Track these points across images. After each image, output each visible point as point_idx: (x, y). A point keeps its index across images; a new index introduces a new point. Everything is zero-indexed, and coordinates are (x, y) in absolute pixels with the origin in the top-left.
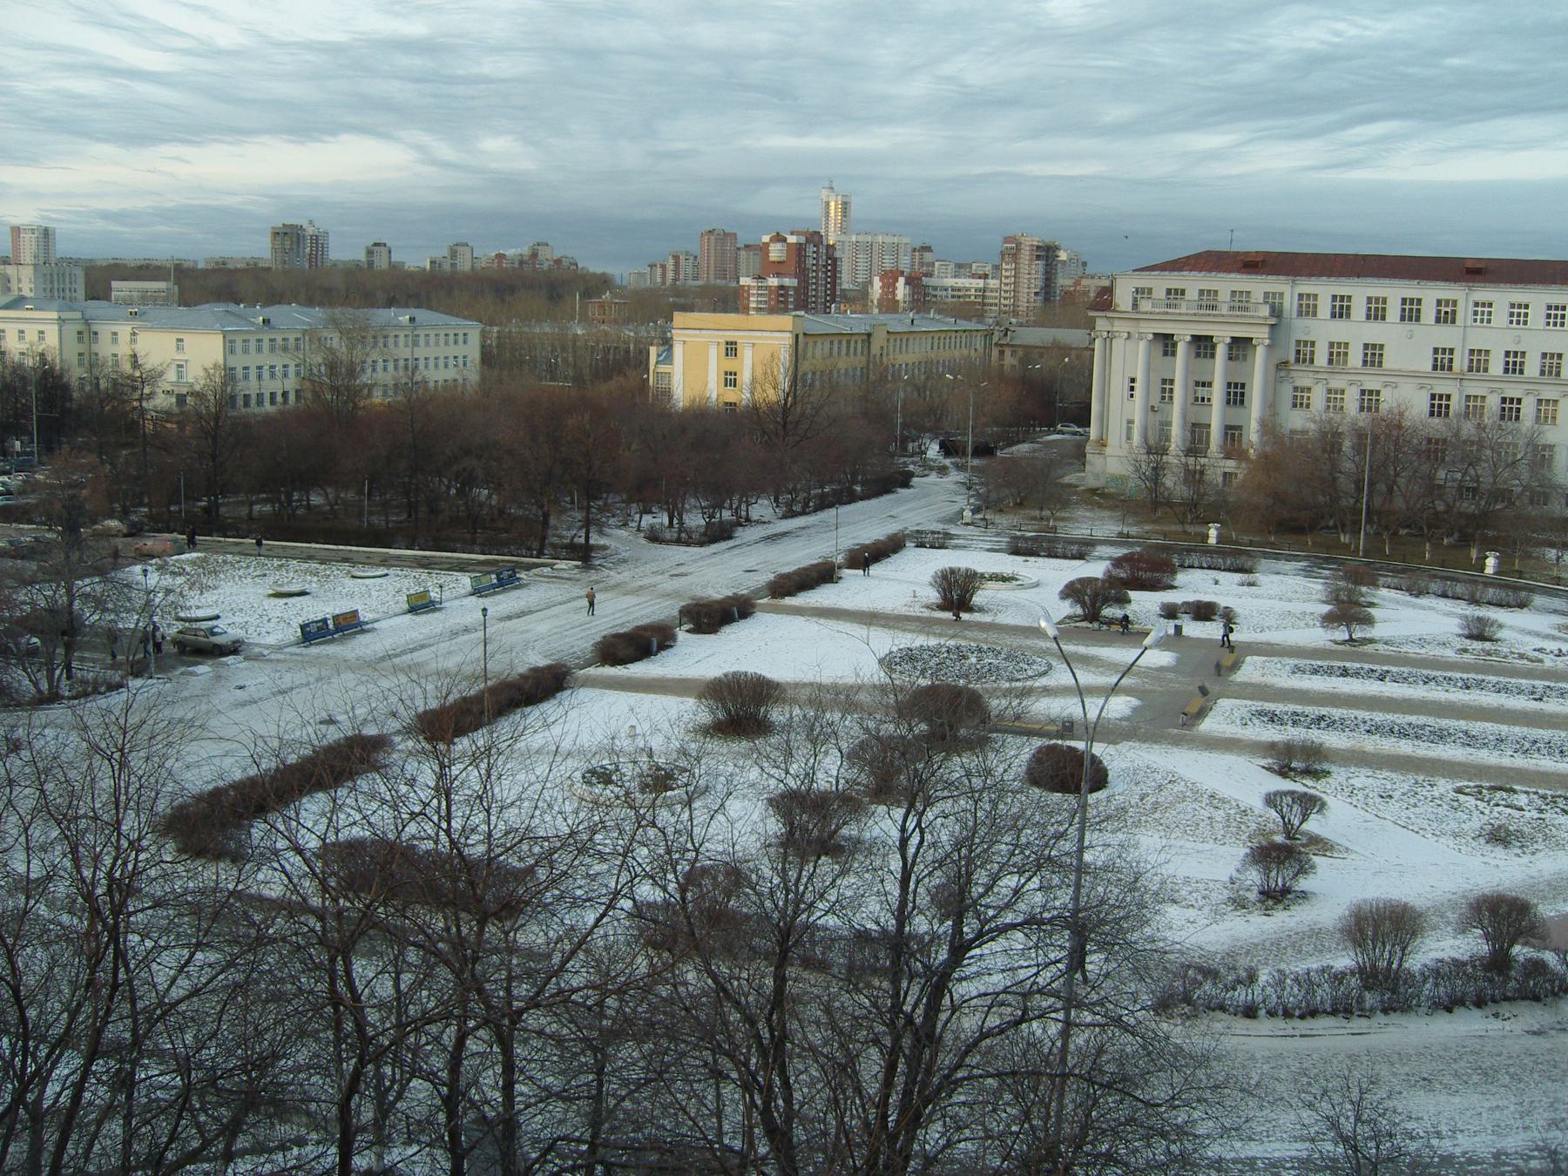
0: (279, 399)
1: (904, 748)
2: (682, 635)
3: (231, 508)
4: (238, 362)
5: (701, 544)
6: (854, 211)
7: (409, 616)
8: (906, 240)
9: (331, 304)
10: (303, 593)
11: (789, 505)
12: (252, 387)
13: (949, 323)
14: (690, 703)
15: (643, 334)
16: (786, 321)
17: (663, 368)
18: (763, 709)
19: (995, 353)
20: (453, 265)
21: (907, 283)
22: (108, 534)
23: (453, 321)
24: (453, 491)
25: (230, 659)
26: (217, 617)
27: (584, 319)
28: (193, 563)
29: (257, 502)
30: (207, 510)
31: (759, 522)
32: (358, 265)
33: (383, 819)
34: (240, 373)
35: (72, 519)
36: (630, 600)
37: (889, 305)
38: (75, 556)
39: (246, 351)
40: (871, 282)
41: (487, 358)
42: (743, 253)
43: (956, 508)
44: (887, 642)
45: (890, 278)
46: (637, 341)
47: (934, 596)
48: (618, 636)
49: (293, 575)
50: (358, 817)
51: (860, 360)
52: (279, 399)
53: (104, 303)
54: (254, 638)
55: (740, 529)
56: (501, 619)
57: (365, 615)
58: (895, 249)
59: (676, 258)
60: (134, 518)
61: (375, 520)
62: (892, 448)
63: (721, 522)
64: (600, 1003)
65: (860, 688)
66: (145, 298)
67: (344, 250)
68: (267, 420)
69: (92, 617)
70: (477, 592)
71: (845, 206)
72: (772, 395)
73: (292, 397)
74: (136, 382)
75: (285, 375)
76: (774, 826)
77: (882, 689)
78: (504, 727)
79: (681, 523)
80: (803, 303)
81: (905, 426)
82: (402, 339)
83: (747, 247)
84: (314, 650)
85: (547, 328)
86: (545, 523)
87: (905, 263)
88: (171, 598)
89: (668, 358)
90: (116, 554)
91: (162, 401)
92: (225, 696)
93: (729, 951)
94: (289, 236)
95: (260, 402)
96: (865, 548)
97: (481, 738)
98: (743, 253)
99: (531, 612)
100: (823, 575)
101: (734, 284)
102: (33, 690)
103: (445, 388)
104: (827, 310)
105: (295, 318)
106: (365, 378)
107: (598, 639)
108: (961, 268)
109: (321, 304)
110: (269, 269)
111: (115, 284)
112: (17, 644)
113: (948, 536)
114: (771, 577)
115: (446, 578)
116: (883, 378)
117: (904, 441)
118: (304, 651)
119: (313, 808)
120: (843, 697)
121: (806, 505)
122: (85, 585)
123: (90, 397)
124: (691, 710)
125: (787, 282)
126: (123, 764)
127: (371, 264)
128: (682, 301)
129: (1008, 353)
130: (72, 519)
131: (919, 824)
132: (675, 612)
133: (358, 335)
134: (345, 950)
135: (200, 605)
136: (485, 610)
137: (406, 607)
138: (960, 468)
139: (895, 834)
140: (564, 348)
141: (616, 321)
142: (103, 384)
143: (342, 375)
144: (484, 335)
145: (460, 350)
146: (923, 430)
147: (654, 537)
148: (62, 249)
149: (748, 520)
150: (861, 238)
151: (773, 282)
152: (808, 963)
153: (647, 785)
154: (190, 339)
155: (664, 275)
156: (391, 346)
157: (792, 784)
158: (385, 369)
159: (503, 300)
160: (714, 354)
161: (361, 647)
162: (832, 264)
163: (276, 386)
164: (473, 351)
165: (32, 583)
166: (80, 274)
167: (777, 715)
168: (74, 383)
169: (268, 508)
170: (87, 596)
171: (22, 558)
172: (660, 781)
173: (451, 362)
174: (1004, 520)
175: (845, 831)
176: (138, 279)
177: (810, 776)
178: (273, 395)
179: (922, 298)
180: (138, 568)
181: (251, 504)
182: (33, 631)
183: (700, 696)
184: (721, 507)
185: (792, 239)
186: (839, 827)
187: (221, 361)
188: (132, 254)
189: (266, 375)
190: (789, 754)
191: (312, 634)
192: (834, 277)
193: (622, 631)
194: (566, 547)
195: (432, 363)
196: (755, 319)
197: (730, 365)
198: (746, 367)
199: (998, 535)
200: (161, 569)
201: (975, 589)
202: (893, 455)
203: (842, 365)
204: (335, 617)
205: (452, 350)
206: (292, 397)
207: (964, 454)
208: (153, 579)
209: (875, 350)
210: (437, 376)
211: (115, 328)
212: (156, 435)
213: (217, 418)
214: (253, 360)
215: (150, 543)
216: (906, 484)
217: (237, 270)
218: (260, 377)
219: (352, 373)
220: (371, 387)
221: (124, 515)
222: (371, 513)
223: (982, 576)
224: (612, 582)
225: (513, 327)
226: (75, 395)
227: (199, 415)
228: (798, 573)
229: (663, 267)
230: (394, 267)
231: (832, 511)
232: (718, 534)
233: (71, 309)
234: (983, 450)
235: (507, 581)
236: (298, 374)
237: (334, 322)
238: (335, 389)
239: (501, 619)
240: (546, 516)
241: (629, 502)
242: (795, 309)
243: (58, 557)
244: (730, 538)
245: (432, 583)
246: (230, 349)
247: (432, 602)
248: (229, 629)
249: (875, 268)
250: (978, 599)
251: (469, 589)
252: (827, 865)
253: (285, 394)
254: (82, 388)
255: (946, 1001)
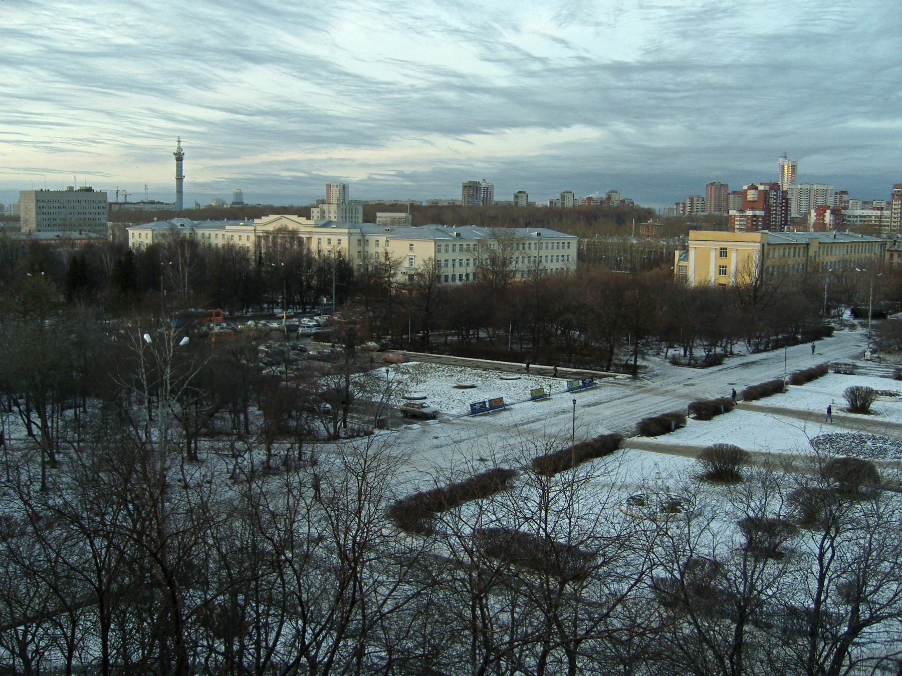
0: (464, 278)
1: (825, 496)
2: (689, 420)
3: (435, 338)
4: (442, 257)
5: (703, 367)
6: (800, 170)
7: (531, 402)
8: (831, 187)
9: (495, 225)
10: (473, 387)
11: (757, 345)
12: (449, 271)
13: (858, 237)
14: (693, 460)
15: (671, 243)
16: (757, 236)
17: (682, 263)
18: (736, 467)
19: (887, 255)
20: (563, 204)
21: (832, 213)
22: (370, 350)
23: (562, 235)
24: (559, 332)
25: (431, 422)
26: (425, 398)
27: (637, 235)
28: (414, 367)
29: (450, 335)
30: (422, 338)
31: (738, 355)
32: (509, 203)
33: (509, 523)
34: (443, 263)
35: (351, 340)
36: (659, 399)
37: (820, 226)
38: (351, 361)
39: (446, 251)
40: (809, 213)
41: (581, 256)
42: (731, 196)
43: (860, 350)
44: (816, 430)
45: (821, 211)
46: (668, 247)
47: (845, 403)
48: (652, 420)
49: (468, 376)
50: (494, 518)
51: (802, 259)
52: (464, 278)
53: (372, 225)
54: (445, 411)
55: (727, 359)
56: (584, 406)
57: (507, 401)
58: (825, 192)
59: (692, 199)
60: (384, 341)
61: (515, 347)
62: (821, 313)
63: (715, 354)
64: (630, 641)
65: (795, 458)
66: (394, 222)
67: (502, 196)
68: (457, 289)
69: (358, 395)
70: (571, 390)
71: (794, 168)
72: (747, 280)
73: (471, 277)
74: (387, 268)
75: (468, 265)
76: (741, 539)
77: (812, 459)
78: (582, 471)
79: (691, 354)
80: (767, 226)
81: (829, 299)
82: (533, 246)
83: (734, 193)
84: (478, 419)
85: (615, 240)
86: (611, 352)
87: (830, 201)
88: (401, 386)
89: (686, 258)
90: (372, 361)
91: (400, 278)
92: (428, 442)
93: (709, 613)
94: (472, 188)
95: (454, 279)
96: (802, 372)
97: (568, 476)
98: (731, 196)
99: (601, 403)
100: (777, 388)
101: (726, 214)
102: (326, 433)
103: (556, 273)
104: (781, 230)
105: (474, 232)
106: (512, 267)
107: (640, 420)
108: (866, 204)
109: (489, 226)
110: (461, 206)
111: (378, 214)
112: (319, 407)
113: (855, 367)
114: (745, 388)
115: (553, 381)
116: (816, 271)
117: (829, 308)
118: (472, 419)
119: (468, 509)
120: (787, 463)
121: (767, 346)
122: (355, 377)
123: (363, 275)
124: (697, 466)
125: (758, 213)
126: (364, 478)
127: (517, 203)
128: (695, 224)
129: (896, 255)
130: (351, 340)
131: (831, 545)
132: (686, 407)
133: (508, 243)
134: (487, 590)
135: (417, 391)
136: (574, 401)
137: (530, 397)
138: (864, 326)
139: (817, 551)
140: (625, 251)
141: (655, 236)
142: (370, 269)
143: (499, 265)
144: (579, 243)
145: (565, 252)
146: (840, 302)
147: (675, 362)
148: (352, 195)
149: (731, 353)
150: (803, 187)
151: (749, 213)
152: (756, 624)
153: (664, 509)
154: (417, 245)
155: (684, 209)
156: (527, 248)
157: (751, 514)
158: (523, 262)
159: (591, 224)
160: (713, 255)
161: (503, 418)
162: (785, 201)
163: (462, 271)
164: (573, 252)
165: (328, 374)
166: (360, 209)
167: (745, 470)
168: (355, 267)
169: (456, 338)
170: (355, 383)
171: (324, 361)
172: (673, 507)
173: (561, 259)
174: (891, 358)
175: (784, 544)
176: (390, 211)
177: (763, 508)
178: (461, 276)
179: (841, 222)
180: (384, 369)
181: (447, 336)
182: (327, 401)
183: (698, 457)
184: (716, 346)
185: (761, 188)
186: (781, 542)
187: (433, 256)
188: (387, 198)
189: (457, 264)
190: (749, 497)
191: (477, 409)
192: (787, 210)
193: (654, 416)
194: (622, 366)
195: (549, 259)
196: (738, 235)
197: (723, 262)
198: (732, 262)
199: (887, 367)
200: (397, 370)
201: (872, 400)
202: (821, 317)
203: (790, 262)
204: (490, 401)
205: (561, 252)
206: (471, 277)
207: (866, 317)
208: (391, 375)
209: (811, 253)
210: (552, 266)
211: (377, 238)
212: (397, 296)
213: (430, 288)
214: (450, 256)
215: (391, 355)
216: (829, 335)
217: (443, 207)
218: (454, 265)
219: (504, 263)
220: (515, 272)
221: (378, 340)
222: (512, 343)
223: (877, 392)
224: (649, 388)
225: (596, 239)
226: (356, 274)
227: (420, 286)
228: (761, 386)
229: (684, 204)
230: (530, 205)
231: (783, 350)
232: (713, 361)
233: (355, 228)
234: (879, 315)
235: (588, 385)
236: (475, 264)
237: (494, 236)
238: (494, 272)
239: (584, 406)
240: (612, 348)
241: (660, 341)
242: (763, 229)
243: (342, 362)
244: (720, 364)
245: (545, 384)
246: (438, 250)
247: (545, 395)
248: (431, 405)
249: (812, 204)
250: (873, 406)
251: (566, 388)
252: (771, 568)
253: (467, 275)
254: (359, 270)
255: (846, 662)
